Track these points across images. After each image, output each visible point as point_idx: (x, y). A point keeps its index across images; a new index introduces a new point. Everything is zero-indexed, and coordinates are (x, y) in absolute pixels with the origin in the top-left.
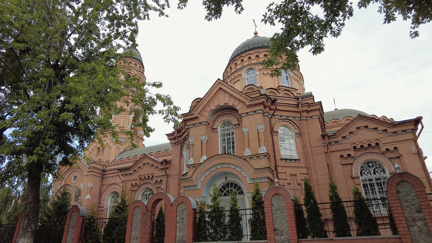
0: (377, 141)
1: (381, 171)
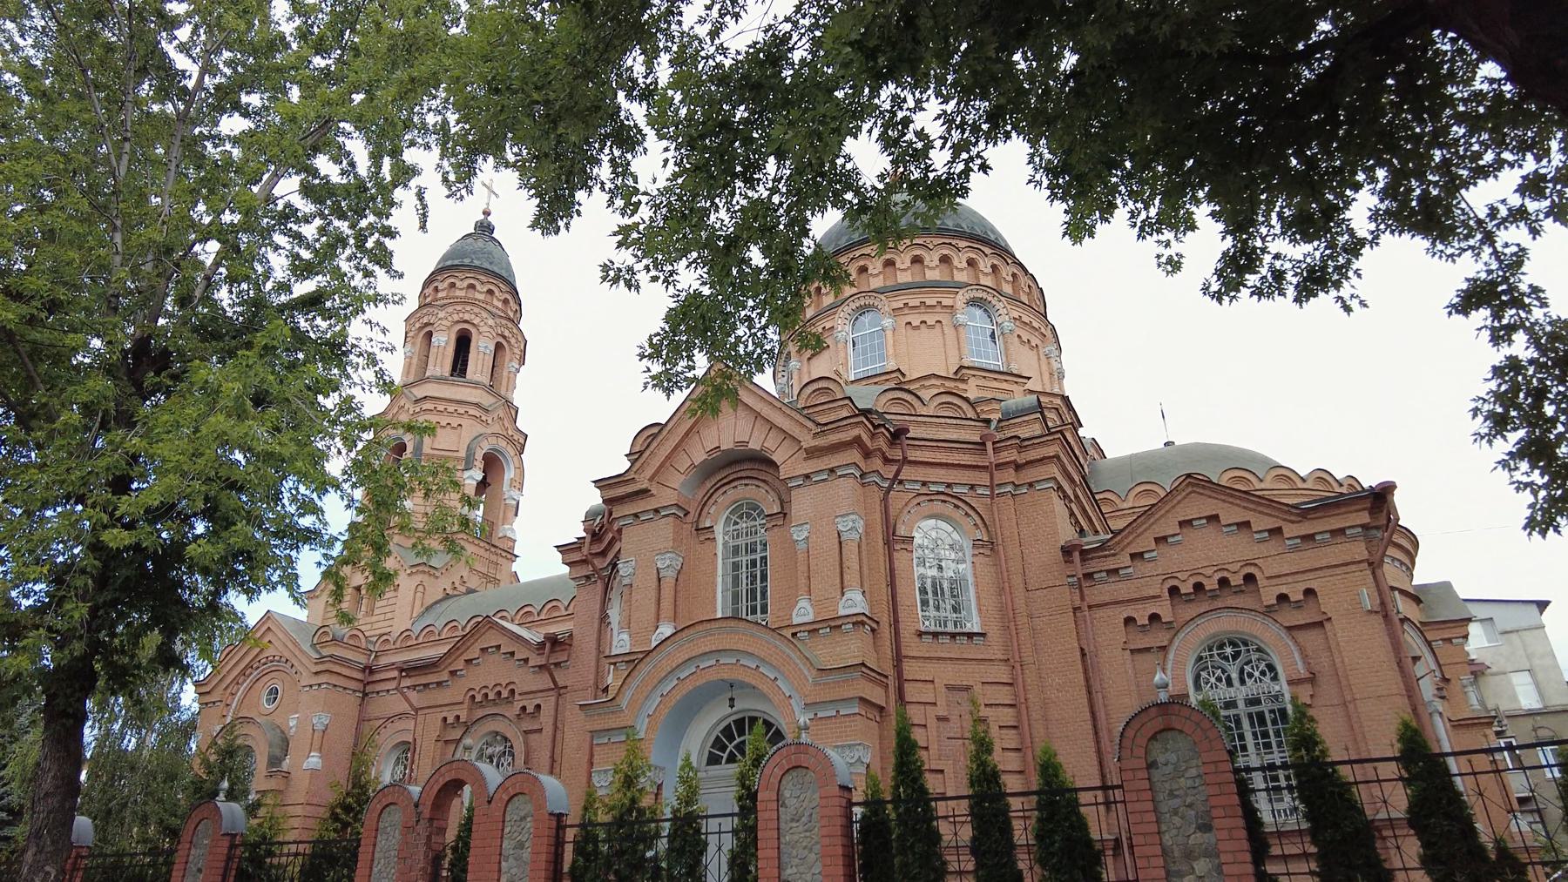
0: (1251, 570)
1: (1263, 673)
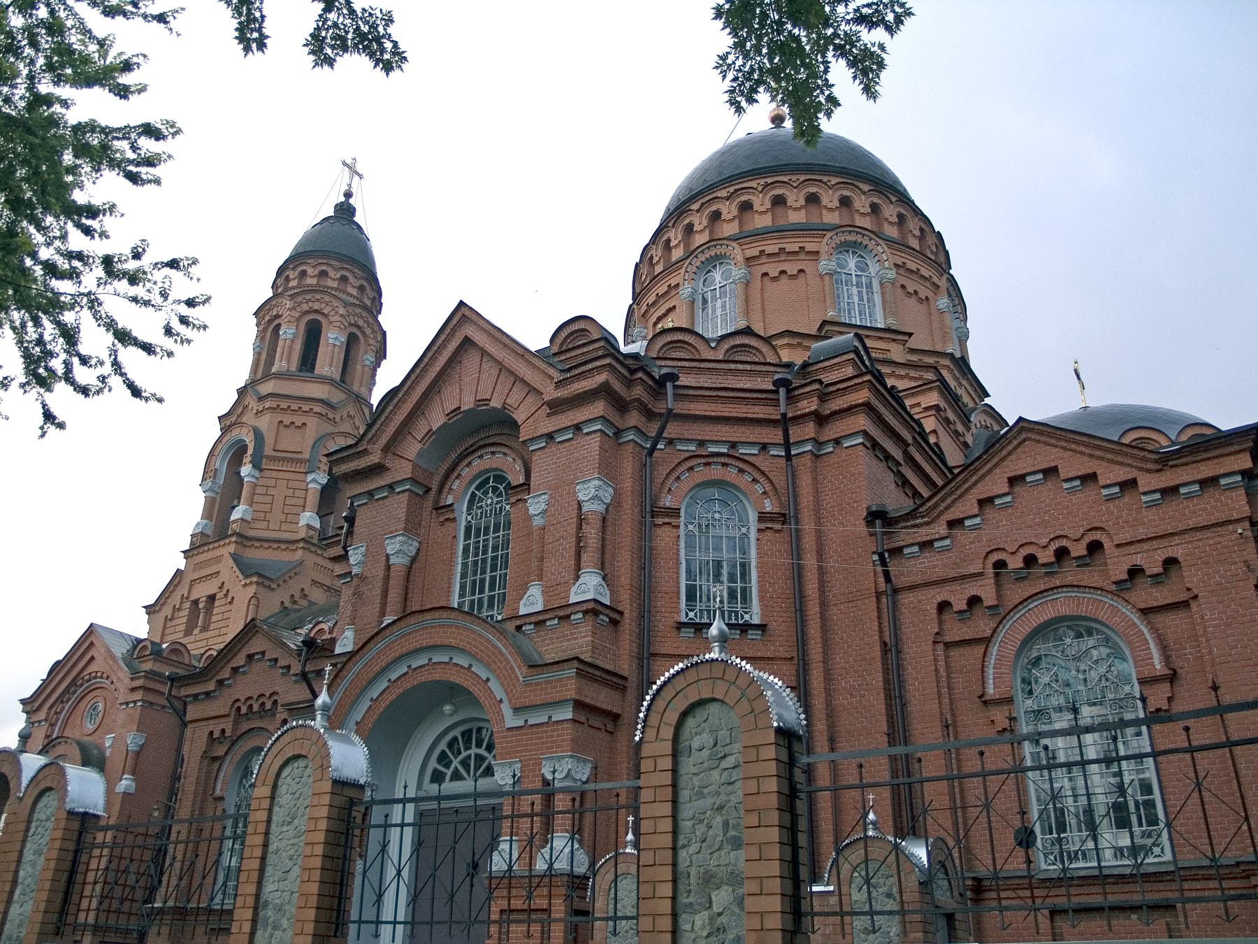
0: (1096, 536)
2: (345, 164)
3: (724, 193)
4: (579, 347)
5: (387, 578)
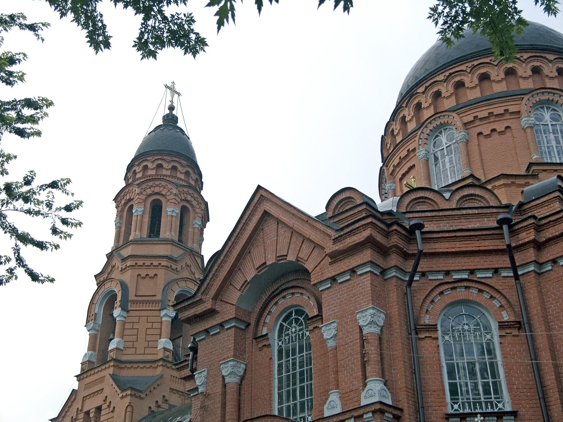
2: (167, 87)
3: (441, 77)
4: (347, 211)
5: (224, 394)
